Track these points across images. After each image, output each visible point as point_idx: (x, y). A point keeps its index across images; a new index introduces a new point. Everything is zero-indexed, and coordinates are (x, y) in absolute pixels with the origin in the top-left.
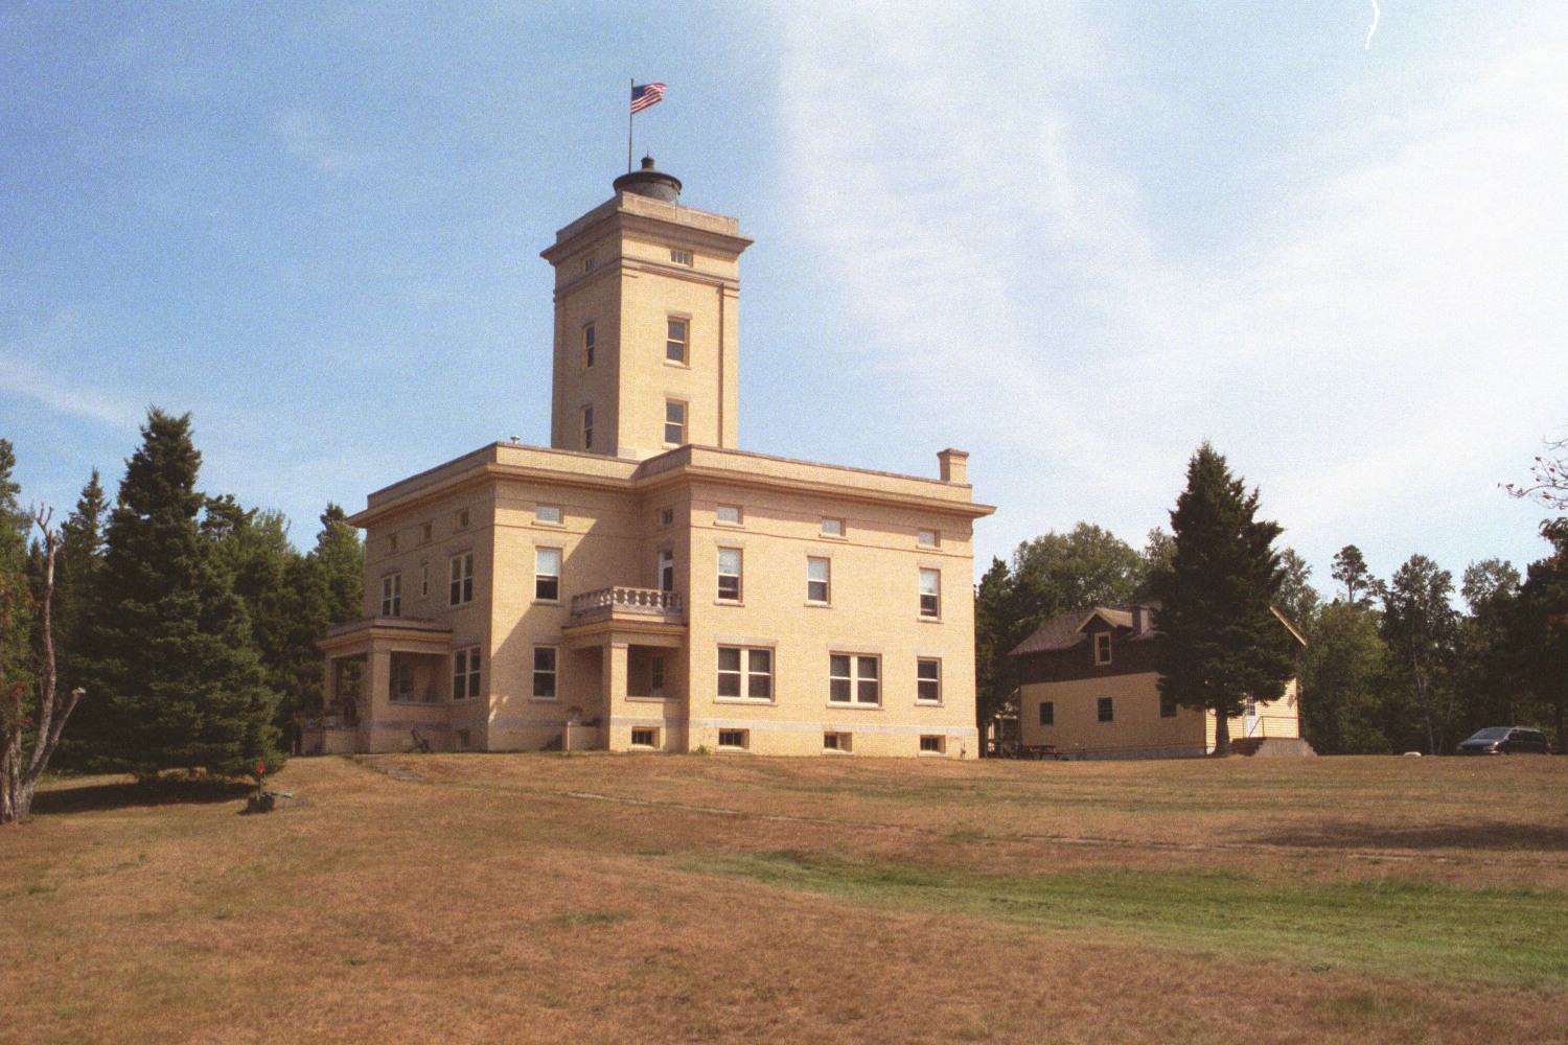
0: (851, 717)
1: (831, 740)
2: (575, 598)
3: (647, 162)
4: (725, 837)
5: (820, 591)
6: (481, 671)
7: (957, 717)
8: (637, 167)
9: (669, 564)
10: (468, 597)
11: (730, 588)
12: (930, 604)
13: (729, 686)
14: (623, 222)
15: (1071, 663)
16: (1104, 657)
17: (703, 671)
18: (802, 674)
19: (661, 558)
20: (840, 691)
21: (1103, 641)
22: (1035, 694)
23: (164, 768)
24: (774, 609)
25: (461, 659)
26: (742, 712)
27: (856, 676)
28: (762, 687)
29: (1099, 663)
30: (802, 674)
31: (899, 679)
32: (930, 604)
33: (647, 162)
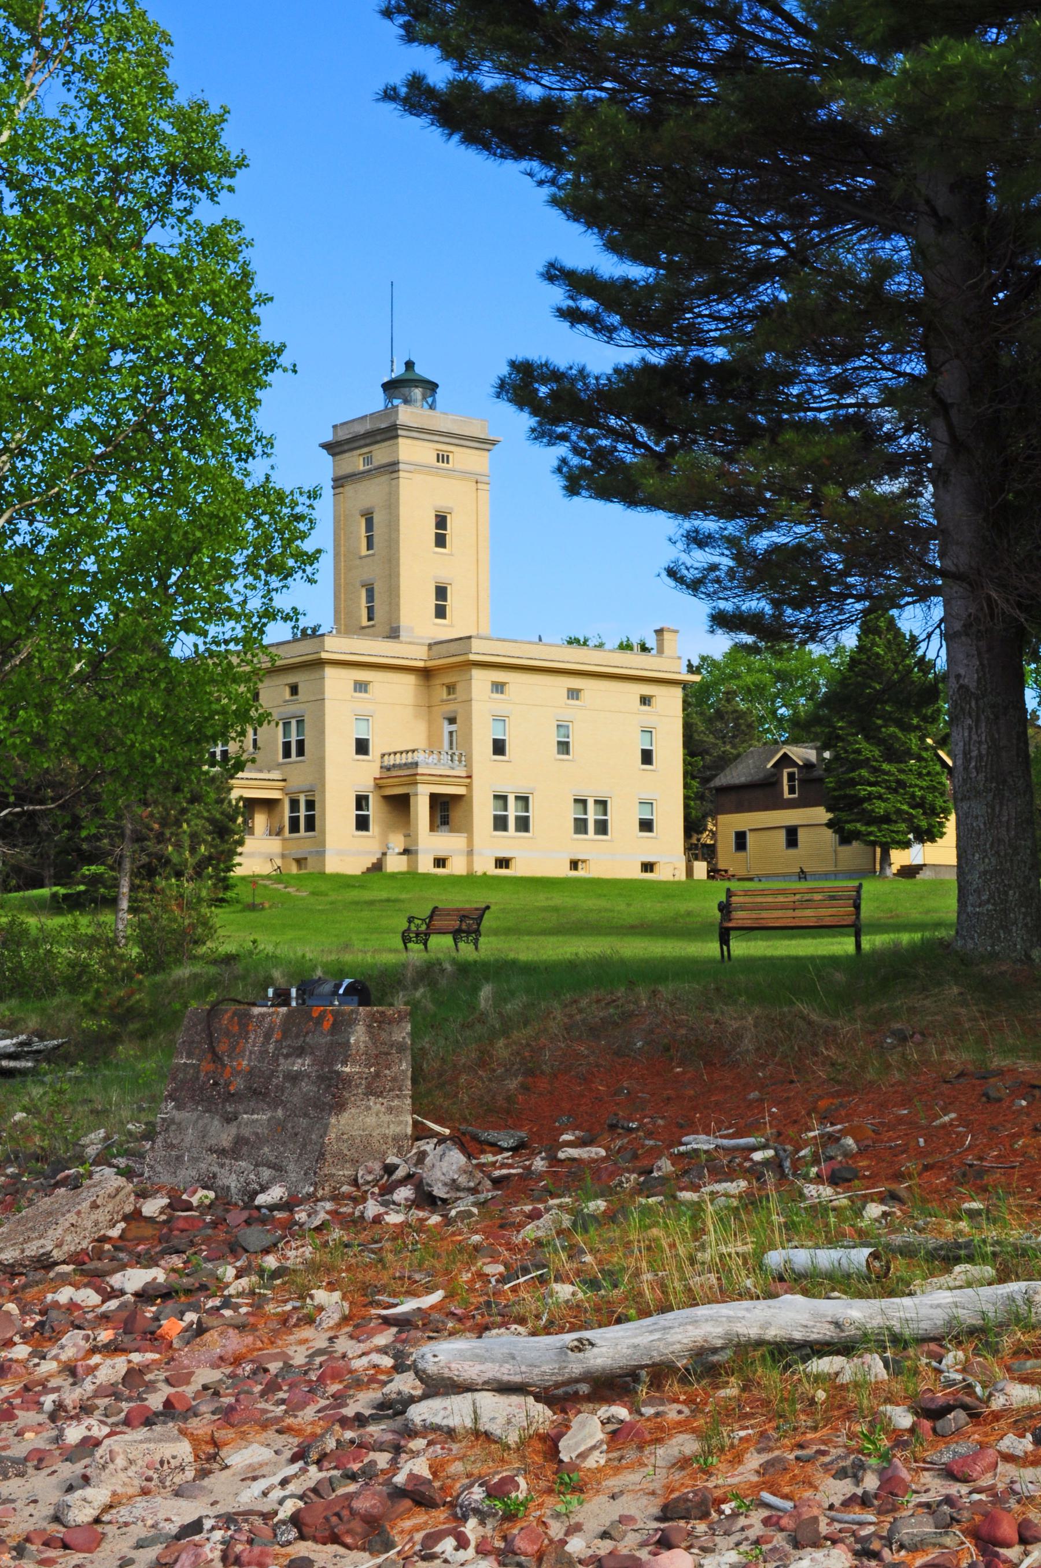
0: (588, 845)
1: (574, 865)
2: (383, 755)
3: (409, 365)
4: (140, 1066)
5: (564, 747)
6: (317, 812)
7: (668, 848)
8: (399, 370)
9: (453, 727)
10: (301, 752)
11: (499, 747)
12: (647, 757)
13: (500, 823)
14: (400, 432)
15: (762, 793)
16: (792, 790)
17: (483, 811)
18: (553, 816)
19: (446, 723)
20: (581, 826)
21: (791, 776)
22: (727, 825)
23: (79, 893)
24: (530, 768)
25: (294, 804)
26: (509, 843)
27: (592, 818)
28: (523, 824)
29: (786, 795)
30: (553, 816)
31: (623, 819)
32: (647, 757)
33: (409, 365)
